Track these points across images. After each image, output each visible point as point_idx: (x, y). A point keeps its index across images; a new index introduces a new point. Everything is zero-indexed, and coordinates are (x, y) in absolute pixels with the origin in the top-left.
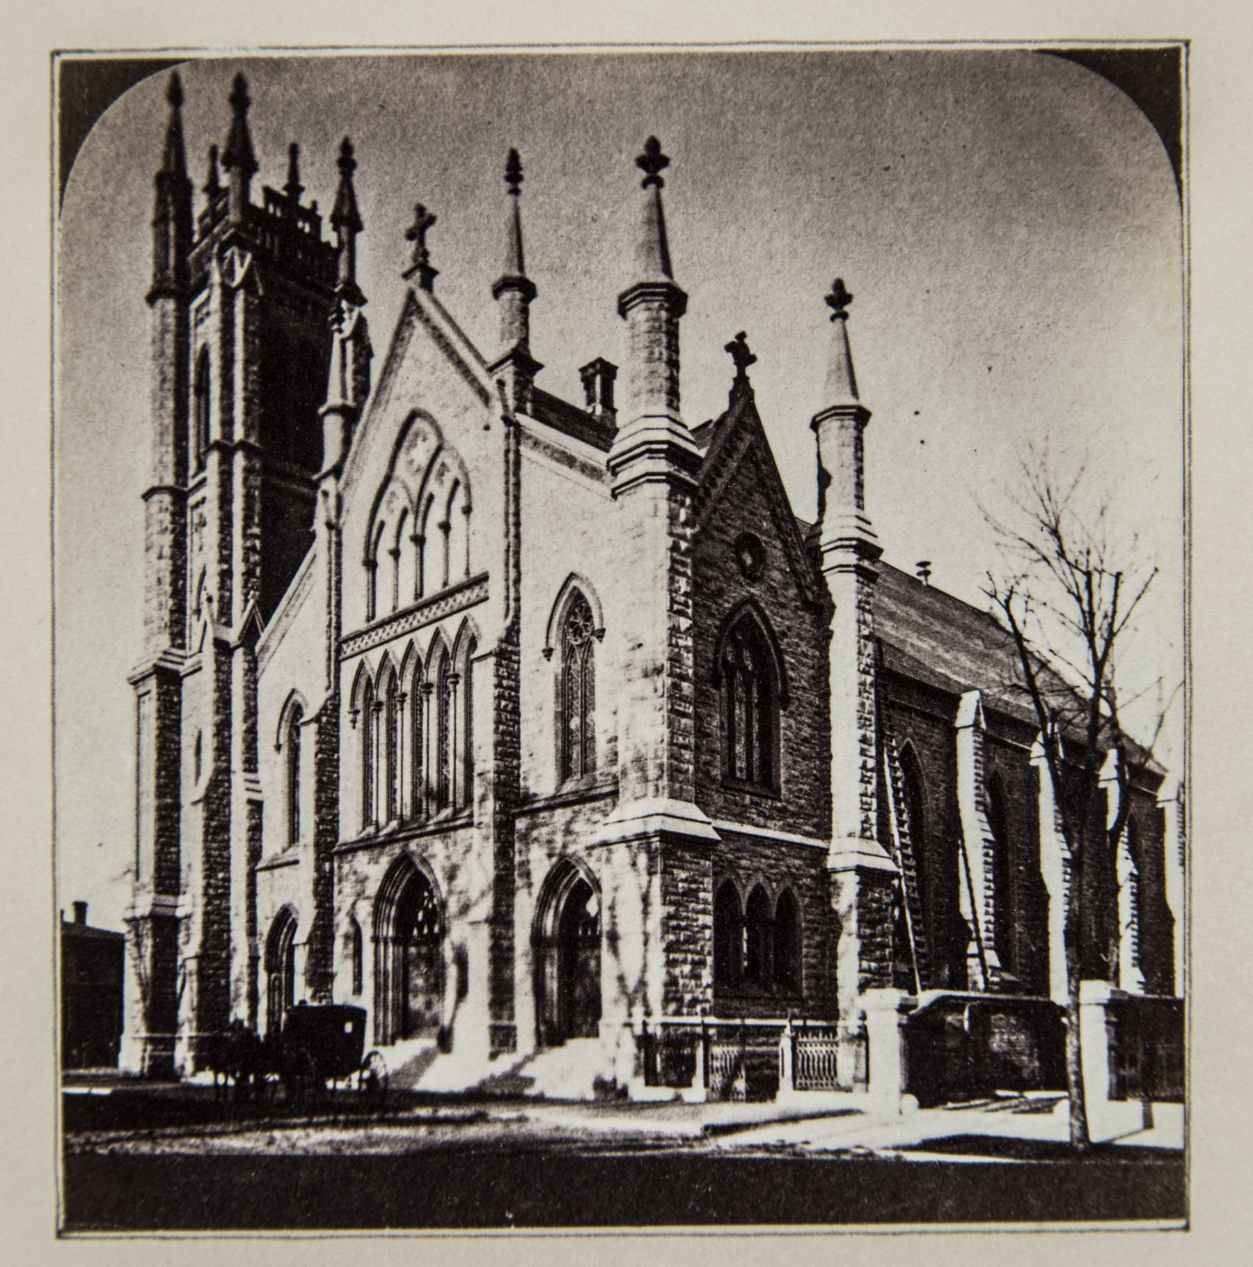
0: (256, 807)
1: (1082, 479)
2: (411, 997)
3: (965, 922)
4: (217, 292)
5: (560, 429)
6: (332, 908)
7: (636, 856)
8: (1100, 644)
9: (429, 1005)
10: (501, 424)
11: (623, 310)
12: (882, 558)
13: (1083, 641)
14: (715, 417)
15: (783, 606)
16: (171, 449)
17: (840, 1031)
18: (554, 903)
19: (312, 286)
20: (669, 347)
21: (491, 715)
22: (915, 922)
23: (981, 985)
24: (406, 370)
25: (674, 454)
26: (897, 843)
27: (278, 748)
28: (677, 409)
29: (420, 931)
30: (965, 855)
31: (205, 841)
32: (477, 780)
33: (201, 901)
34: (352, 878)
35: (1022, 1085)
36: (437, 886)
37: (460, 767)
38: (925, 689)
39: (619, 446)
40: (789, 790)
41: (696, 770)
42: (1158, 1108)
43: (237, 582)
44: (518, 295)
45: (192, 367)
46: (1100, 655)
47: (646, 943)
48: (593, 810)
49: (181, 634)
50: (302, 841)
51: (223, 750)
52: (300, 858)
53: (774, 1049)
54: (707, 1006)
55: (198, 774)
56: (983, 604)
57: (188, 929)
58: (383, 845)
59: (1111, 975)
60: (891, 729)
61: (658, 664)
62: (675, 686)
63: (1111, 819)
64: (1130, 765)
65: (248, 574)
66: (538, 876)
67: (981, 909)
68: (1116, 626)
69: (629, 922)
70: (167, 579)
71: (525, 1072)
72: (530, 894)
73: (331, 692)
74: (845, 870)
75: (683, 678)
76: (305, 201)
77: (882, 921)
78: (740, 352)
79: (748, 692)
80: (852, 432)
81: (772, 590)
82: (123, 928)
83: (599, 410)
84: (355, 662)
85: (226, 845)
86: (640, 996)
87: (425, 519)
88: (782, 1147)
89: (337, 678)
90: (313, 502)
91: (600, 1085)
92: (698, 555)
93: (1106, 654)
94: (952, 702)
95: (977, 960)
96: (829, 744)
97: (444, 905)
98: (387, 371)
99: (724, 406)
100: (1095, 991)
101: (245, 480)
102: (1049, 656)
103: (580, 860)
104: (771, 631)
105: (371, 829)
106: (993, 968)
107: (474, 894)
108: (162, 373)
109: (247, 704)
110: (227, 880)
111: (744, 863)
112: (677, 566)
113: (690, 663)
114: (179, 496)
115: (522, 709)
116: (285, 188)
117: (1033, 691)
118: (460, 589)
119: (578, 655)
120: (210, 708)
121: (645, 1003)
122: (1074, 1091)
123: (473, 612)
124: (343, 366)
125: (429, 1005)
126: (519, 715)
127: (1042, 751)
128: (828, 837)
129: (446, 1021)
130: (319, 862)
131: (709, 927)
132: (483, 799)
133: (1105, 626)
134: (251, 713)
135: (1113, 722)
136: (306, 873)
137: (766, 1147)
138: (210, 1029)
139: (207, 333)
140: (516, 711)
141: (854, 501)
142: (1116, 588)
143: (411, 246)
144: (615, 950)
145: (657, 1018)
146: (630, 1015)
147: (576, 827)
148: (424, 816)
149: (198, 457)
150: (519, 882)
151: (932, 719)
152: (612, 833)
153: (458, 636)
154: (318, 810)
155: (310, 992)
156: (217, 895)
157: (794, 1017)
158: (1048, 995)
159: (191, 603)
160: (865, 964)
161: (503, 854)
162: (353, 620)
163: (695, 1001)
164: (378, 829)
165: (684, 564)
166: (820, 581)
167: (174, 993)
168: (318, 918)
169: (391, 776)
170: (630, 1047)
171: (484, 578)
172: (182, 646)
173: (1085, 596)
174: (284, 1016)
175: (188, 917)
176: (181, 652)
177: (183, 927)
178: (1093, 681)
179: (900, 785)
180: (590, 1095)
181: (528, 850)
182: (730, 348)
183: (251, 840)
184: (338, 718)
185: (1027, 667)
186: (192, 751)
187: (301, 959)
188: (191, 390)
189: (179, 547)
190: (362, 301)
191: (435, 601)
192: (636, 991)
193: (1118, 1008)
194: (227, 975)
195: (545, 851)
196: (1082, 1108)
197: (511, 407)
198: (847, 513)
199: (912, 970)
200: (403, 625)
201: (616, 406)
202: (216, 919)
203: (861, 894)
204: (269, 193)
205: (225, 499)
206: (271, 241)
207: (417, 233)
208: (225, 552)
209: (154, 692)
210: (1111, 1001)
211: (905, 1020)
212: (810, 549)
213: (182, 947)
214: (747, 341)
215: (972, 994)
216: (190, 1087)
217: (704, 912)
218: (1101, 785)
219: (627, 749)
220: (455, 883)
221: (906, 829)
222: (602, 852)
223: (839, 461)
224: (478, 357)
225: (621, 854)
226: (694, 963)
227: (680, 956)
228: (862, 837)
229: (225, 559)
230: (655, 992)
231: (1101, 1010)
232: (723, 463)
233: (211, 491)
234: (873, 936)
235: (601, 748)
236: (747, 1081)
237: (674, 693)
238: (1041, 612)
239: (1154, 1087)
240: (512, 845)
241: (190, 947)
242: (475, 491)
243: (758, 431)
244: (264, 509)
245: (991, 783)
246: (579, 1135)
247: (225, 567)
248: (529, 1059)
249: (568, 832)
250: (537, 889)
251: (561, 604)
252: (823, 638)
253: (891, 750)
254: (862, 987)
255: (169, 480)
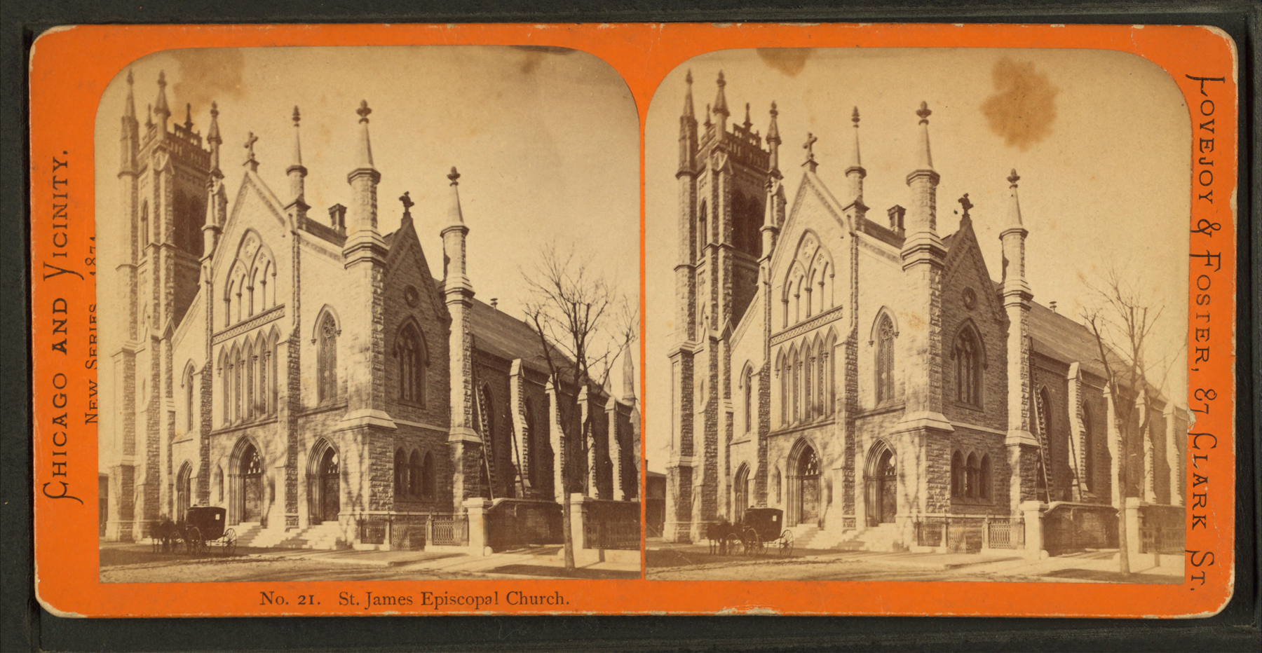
0: (730, 415)
1: (571, 261)
2: (247, 502)
3: (514, 466)
4: (710, 174)
5: (319, 237)
6: (209, 461)
7: (913, 438)
8: (1137, 341)
9: (256, 506)
10: (291, 234)
11: (909, 182)
12: (1033, 300)
13: (1129, 339)
14: (953, 233)
15: (985, 321)
16: (688, 247)
17: (454, 517)
18: (874, 460)
19: (756, 170)
20: (372, 199)
21: (844, 371)
22: (490, 466)
23: (1079, 499)
24: (244, 212)
25: (933, 250)
26: (482, 429)
27: (741, 387)
28: (376, 227)
29: (809, 473)
30: (1071, 439)
31: (706, 431)
32: (837, 403)
33: (703, 459)
34: (776, 448)
35: (1098, 546)
36: (260, 450)
37: (829, 396)
38: (498, 359)
39: (348, 244)
40: (988, 408)
41: (386, 395)
42: (1162, 557)
43: (721, 309)
44: (858, 175)
45: (698, 208)
46: (1137, 346)
47: (918, 479)
48: (894, 416)
49: (693, 334)
50: (194, 430)
51: (714, 388)
52: (193, 438)
53: (979, 529)
54: (947, 508)
55: (144, 398)
56: (1081, 322)
57: (697, 472)
58: (791, 432)
59: (1141, 495)
60: (1036, 379)
61: (925, 348)
62: (933, 359)
63: (1141, 423)
64: (1150, 397)
65: (726, 306)
66: (867, 446)
67: (521, 458)
68: (1144, 333)
69: (353, 467)
70: (686, 308)
71: (861, 539)
72: (305, 454)
73: (766, 361)
74: (1015, 445)
75: (379, 353)
76: (753, 130)
77: (475, 466)
78: (406, 201)
79: (968, 363)
80: (461, 238)
81: (422, 312)
82: (664, 472)
83: (338, 228)
84: (777, 348)
85: (715, 433)
86: (915, 504)
87: (253, 280)
88: (983, 575)
89: (769, 354)
90: (199, 271)
91: (339, 542)
92: (944, 298)
93: (1139, 345)
94: (1066, 367)
95: (520, 484)
96: (1007, 386)
97: (263, 459)
98: (235, 210)
99: (957, 228)
100: (1133, 502)
101: (724, 262)
102: (1113, 346)
103: (886, 440)
104: (979, 334)
105: (228, 424)
106: (528, 487)
107: (836, 456)
108: (683, 211)
109: (725, 367)
110: (716, 449)
111: (965, 442)
112: (376, 301)
113: (940, 347)
114: (692, 269)
115: (301, 368)
116: (185, 124)
117: (1105, 362)
118: (829, 313)
119: (886, 343)
120: (708, 369)
121: (361, 504)
122: (1123, 549)
123: (277, 321)
124: (772, 208)
125: (256, 506)
126: (857, 371)
127: (552, 386)
128: (1006, 430)
129: (821, 516)
130: (760, 440)
131: (391, 469)
132: (282, 410)
133: (1139, 332)
134: (170, 370)
135: (1143, 377)
136: (196, 444)
137: (975, 575)
138: (707, 519)
139: (705, 193)
140: (298, 368)
141: (461, 270)
142: (1145, 314)
143: (247, 150)
144: (346, 481)
145: (924, 514)
146: (354, 510)
147: (885, 424)
148: (811, 419)
149: (701, 251)
150: (299, 449)
151: (501, 372)
152: (902, 427)
153: (828, 335)
154: (760, 416)
155: (198, 500)
156: (711, 455)
157: (990, 514)
158: (1110, 503)
159: (698, 319)
160: (1023, 489)
161: (292, 435)
162: (219, 326)
163: (941, 506)
164: (789, 426)
165: (380, 300)
166: (445, 307)
167: (690, 503)
168: (759, 467)
169: (795, 401)
170: (353, 525)
171: (283, 307)
172: (694, 340)
173: (573, 315)
174: (743, 513)
175: (697, 467)
176: (135, 342)
177: (694, 471)
178: (1133, 357)
179: (1041, 405)
180: (891, 550)
181: (862, 435)
182: (401, 199)
183: (728, 430)
184: (211, 372)
185: (1102, 351)
186: (141, 387)
187: (194, 486)
188: (698, 219)
189: (692, 293)
190: (223, 177)
191: (258, 317)
192: (914, 502)
193: (1144, 511)
194: (716, 494)
195: (312, 434)
196: (1127, 557)
197: (854, 228)
198: (1016, 278)
199: (489, 488)
200: (801, 330)
201: (905, 227)
202: (711, 469)
203: (1022, 456)
204: (177, 127)
205: (715, 271)
206: (178, 149)
207: (809, 146)
208: (156, 295)
209: (680, 362)
210: (1140, 507)
211: (486, 511)
212: (998, 296)
213: (694, 481)
214: (969, 197)
215: (1074, 503)
216: (698, 547)
217: (389, 462)
218: (1137, 407)
219: (910, 388)
220: (826, 450)
221: (1043, 426)
222: (898, 436)
223: (1013, 256)
224: (838, 204)
225: (906, 437)
226: (941, 488)
227: (378, 483)
228: (1022, 429)
229: (715, 299)
230: (366, 499)
231: (1135, 511)
232: (957, 255)
233: (708, 267)
234: (1027, 476)
235: (340, 383)
236: (411, 540)
237: (375, 360)
238: (552, 322)
239: (1160, 548)
240: (854, 432)
241: (698, 480)
242: (278, 266)
243: (974, 240)
244: (175, 274)
245: (1085, 407)
246: (886, 569)
247: (157, 302)
248: (861, 533)
249: (324, 425)
250: (308, 452)
251: (319, 321)
252: (1005, 337)
253: (479, 386)
254: (1022, 500)
255: (687, 262)
